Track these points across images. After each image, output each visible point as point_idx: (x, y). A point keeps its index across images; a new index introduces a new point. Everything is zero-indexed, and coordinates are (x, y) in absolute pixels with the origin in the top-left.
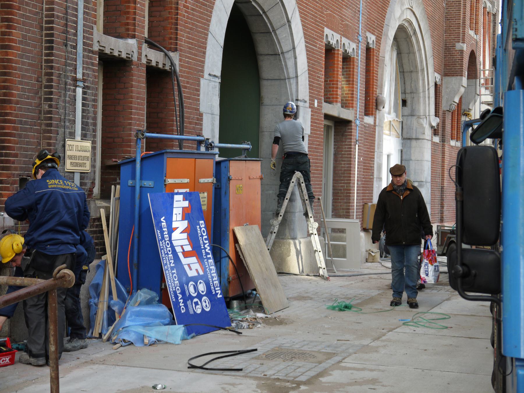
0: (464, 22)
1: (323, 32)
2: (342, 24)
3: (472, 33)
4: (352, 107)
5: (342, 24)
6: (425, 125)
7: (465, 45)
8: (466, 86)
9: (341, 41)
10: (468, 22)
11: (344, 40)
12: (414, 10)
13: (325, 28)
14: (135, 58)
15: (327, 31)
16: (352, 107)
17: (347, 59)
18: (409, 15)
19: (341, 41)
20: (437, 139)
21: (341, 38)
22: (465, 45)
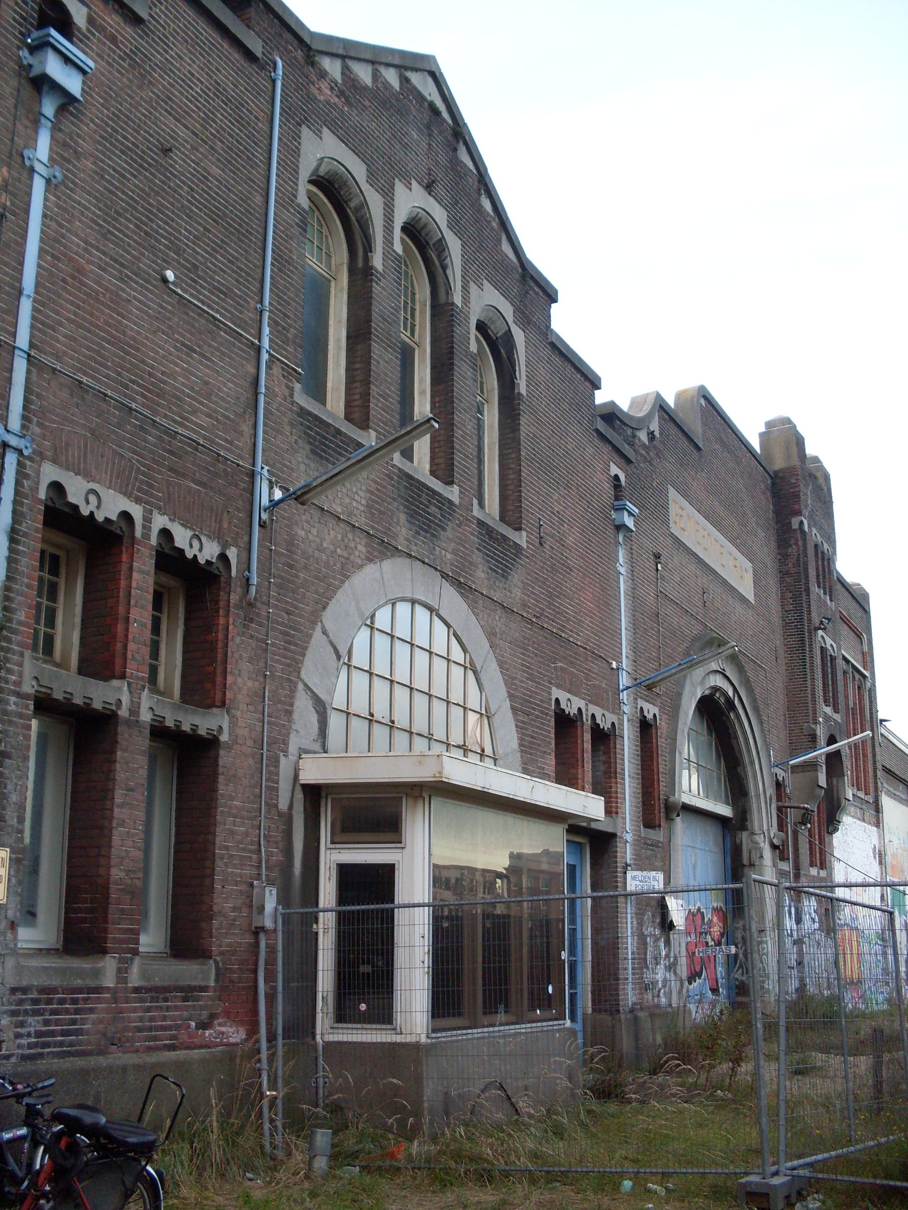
0: (813, 695)
1: (550, 693)
2: (587, 685)
3: (828, 710)
4: (223, 704)
5: (587, 685)
6: (762, 845)
7: (524, 533)
8: (825, 786)
9: (587, 710)
10: (820, 693)
11: (594, 709)
12: (727, 674)
13: (554, 689)
14: (123, 712)
15: (556, 693)
16: (223, 704)
17: (603, 739)
18: (719, 681)
19: (587, 710)
20: (784, 866)
21: (587, 705)
22: (524, 533)
